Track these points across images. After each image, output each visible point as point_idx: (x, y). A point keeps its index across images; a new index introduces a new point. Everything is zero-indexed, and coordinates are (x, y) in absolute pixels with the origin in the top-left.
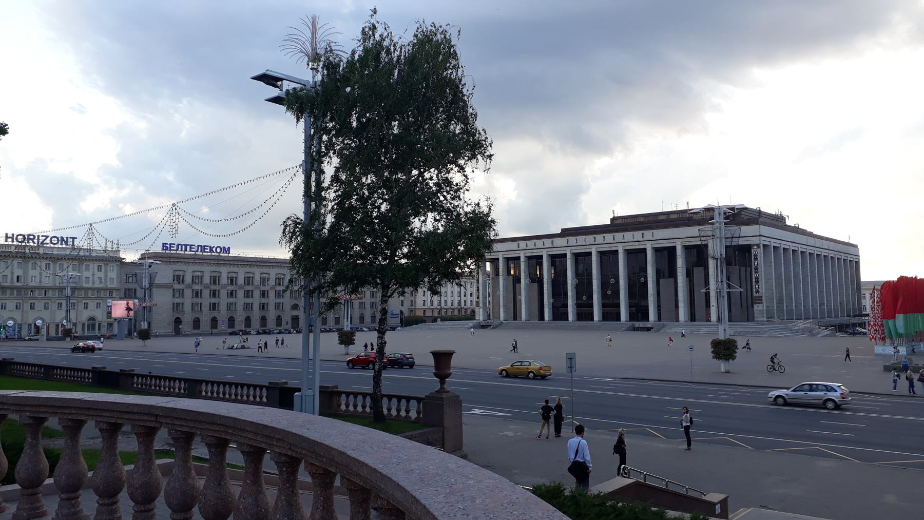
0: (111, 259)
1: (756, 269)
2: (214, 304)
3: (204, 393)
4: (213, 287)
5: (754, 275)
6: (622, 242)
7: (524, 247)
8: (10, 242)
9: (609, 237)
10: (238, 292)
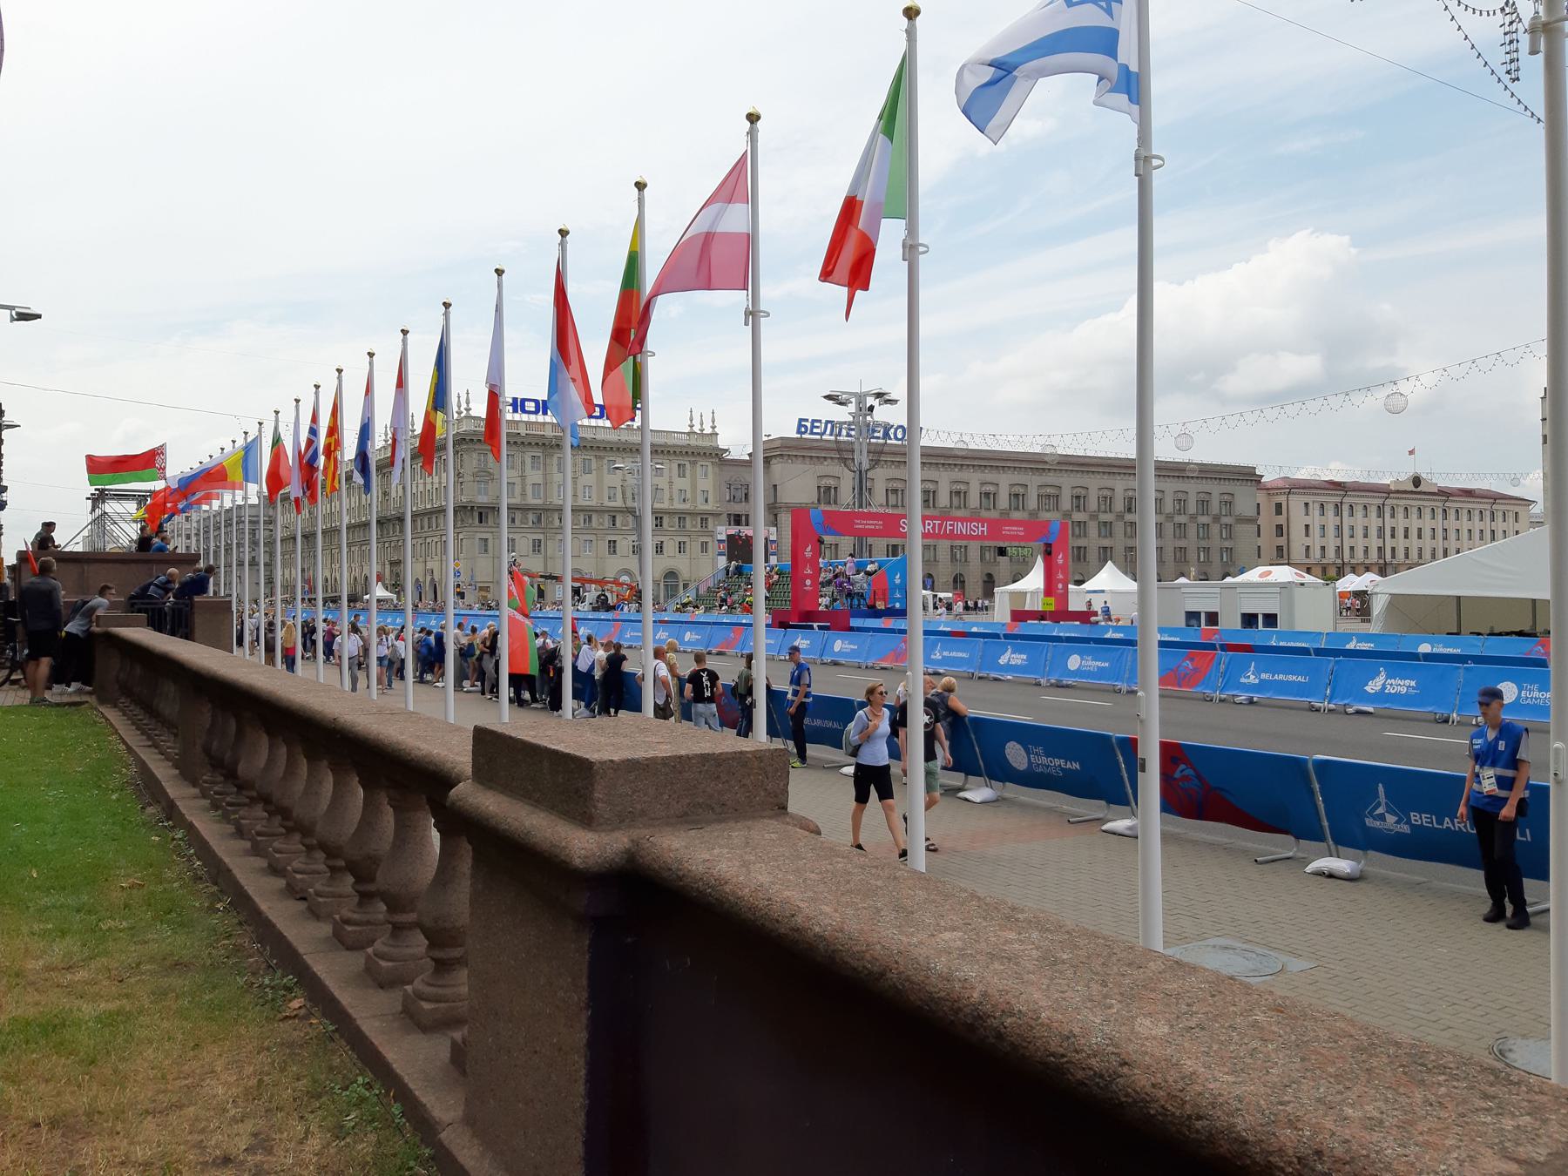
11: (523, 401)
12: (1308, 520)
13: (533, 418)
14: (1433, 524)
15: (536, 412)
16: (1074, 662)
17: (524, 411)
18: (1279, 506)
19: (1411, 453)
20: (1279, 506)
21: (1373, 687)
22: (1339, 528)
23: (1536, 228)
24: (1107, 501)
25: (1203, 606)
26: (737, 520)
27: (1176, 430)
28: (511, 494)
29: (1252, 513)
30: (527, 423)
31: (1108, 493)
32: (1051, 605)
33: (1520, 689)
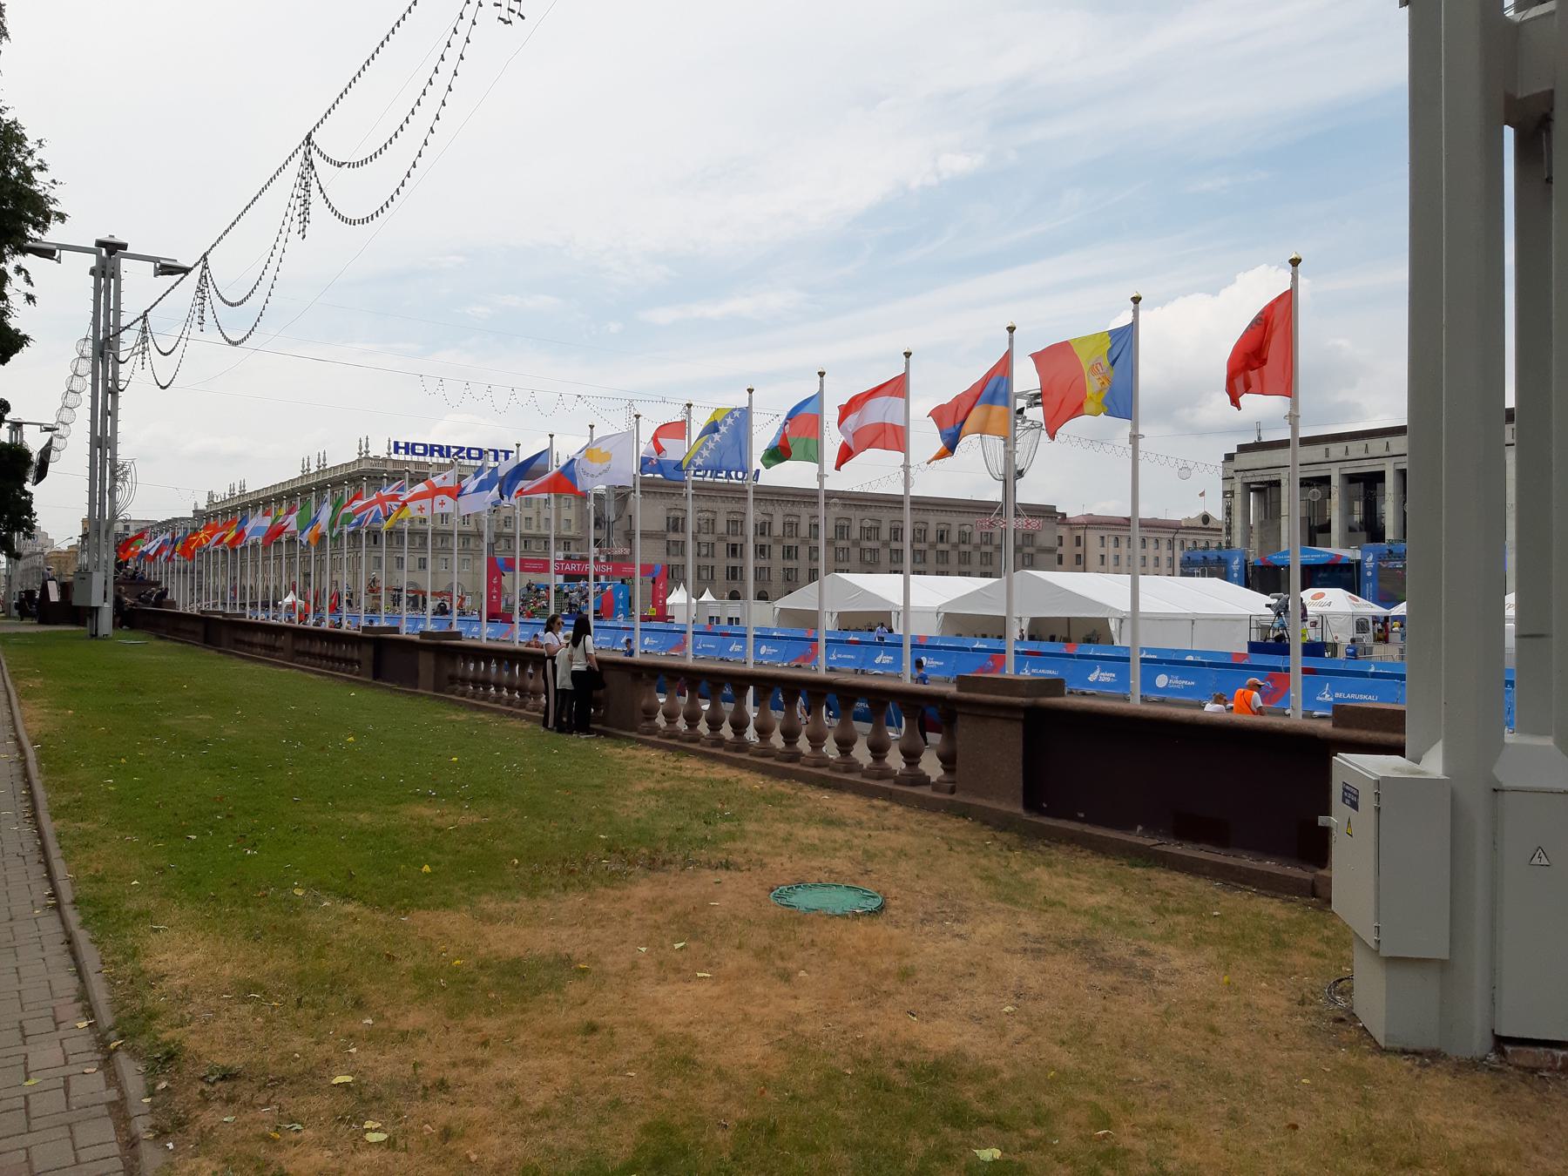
0: (565, 482)
2: (734, 568)
3: (661, 721)
4: (733, 540)
7: (1342, 456)
8: (401, 456)
11: (414, 445)
12: (1103, 551)
13: (421, 459)
15: (424, 454)
17: (414, 453)
19: (1202, 494)
20: (1078, 538)
21: (1092, 678)
23: (1400, 275)
24: (791, 527)
30: (417, 463)
31: (923, 526)
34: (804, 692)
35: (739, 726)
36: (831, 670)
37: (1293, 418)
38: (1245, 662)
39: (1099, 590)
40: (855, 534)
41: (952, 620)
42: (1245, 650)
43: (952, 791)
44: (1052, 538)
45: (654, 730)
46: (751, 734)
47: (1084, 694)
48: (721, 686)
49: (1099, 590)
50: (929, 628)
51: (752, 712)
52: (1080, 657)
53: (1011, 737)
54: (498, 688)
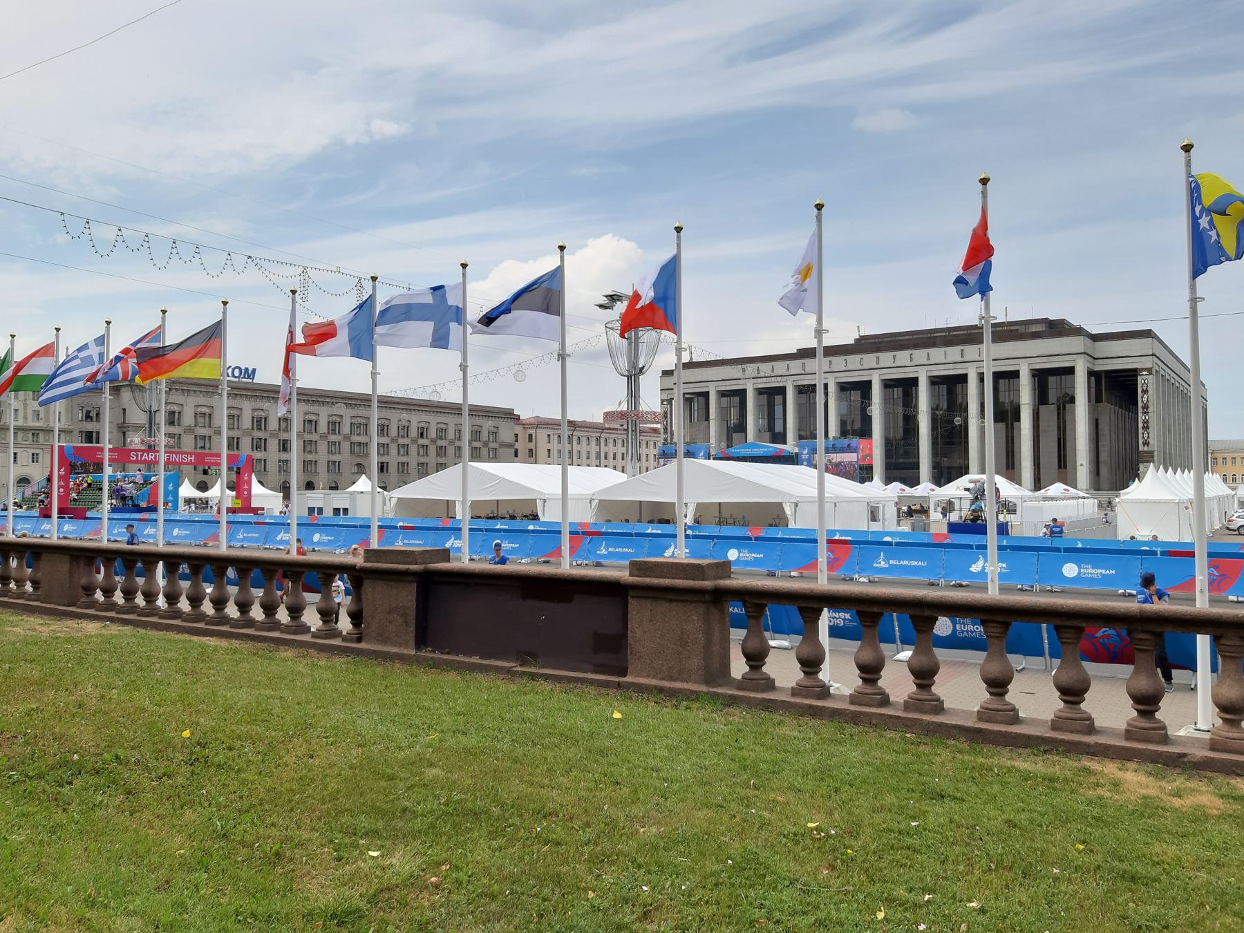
1: (1146, 407)
5: (1141, 417)
6: (878, 369)
7: (769, 373)
9: (854, 361)
10: (270, 442)
14: (615, 449)
16: (1070, 570)
18: (530, 436)
20: (530, 436)
22: (571, 452)
25: (341, 506)
26: (89, 436)
27: (514, 370)
28: (16, 418)
29: (511, 440)
32: (238, 504)
33: (1080, 568)
34: (119, 560)
35: (150, 596)
36: (169, 544)
37: (819, 333)
38: (948, 541)
39: (532, 479)
40: (346, 429)
41: (607, 507)
42: (945, 531)
43: (359, 640)
44: (499, 434)
45: (94, 604)
46: (161, 602)
47: (961, 586)
48: (135, 562)
49: (532, 479)
50: (584, 515)
51: (233, 590)
52: (638, 535)
53: (407, 597)
54: (20, 583)
